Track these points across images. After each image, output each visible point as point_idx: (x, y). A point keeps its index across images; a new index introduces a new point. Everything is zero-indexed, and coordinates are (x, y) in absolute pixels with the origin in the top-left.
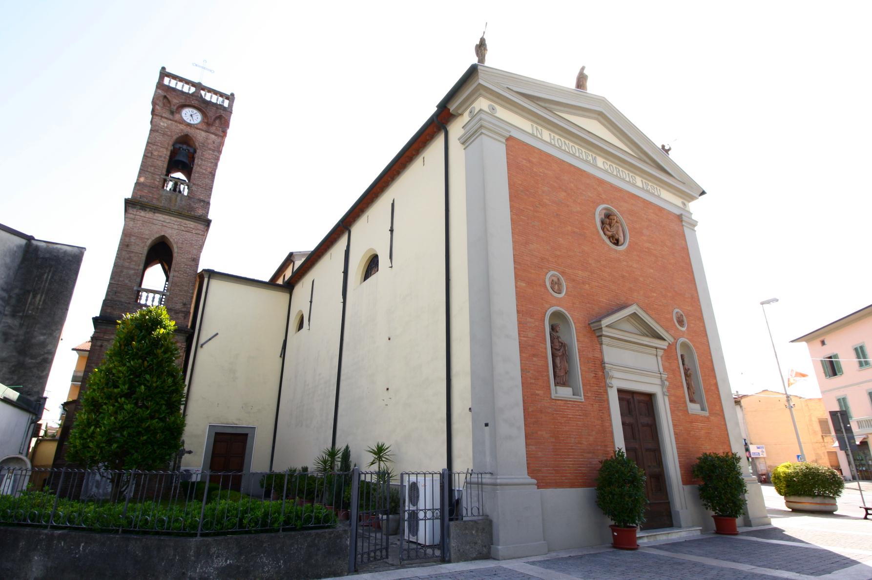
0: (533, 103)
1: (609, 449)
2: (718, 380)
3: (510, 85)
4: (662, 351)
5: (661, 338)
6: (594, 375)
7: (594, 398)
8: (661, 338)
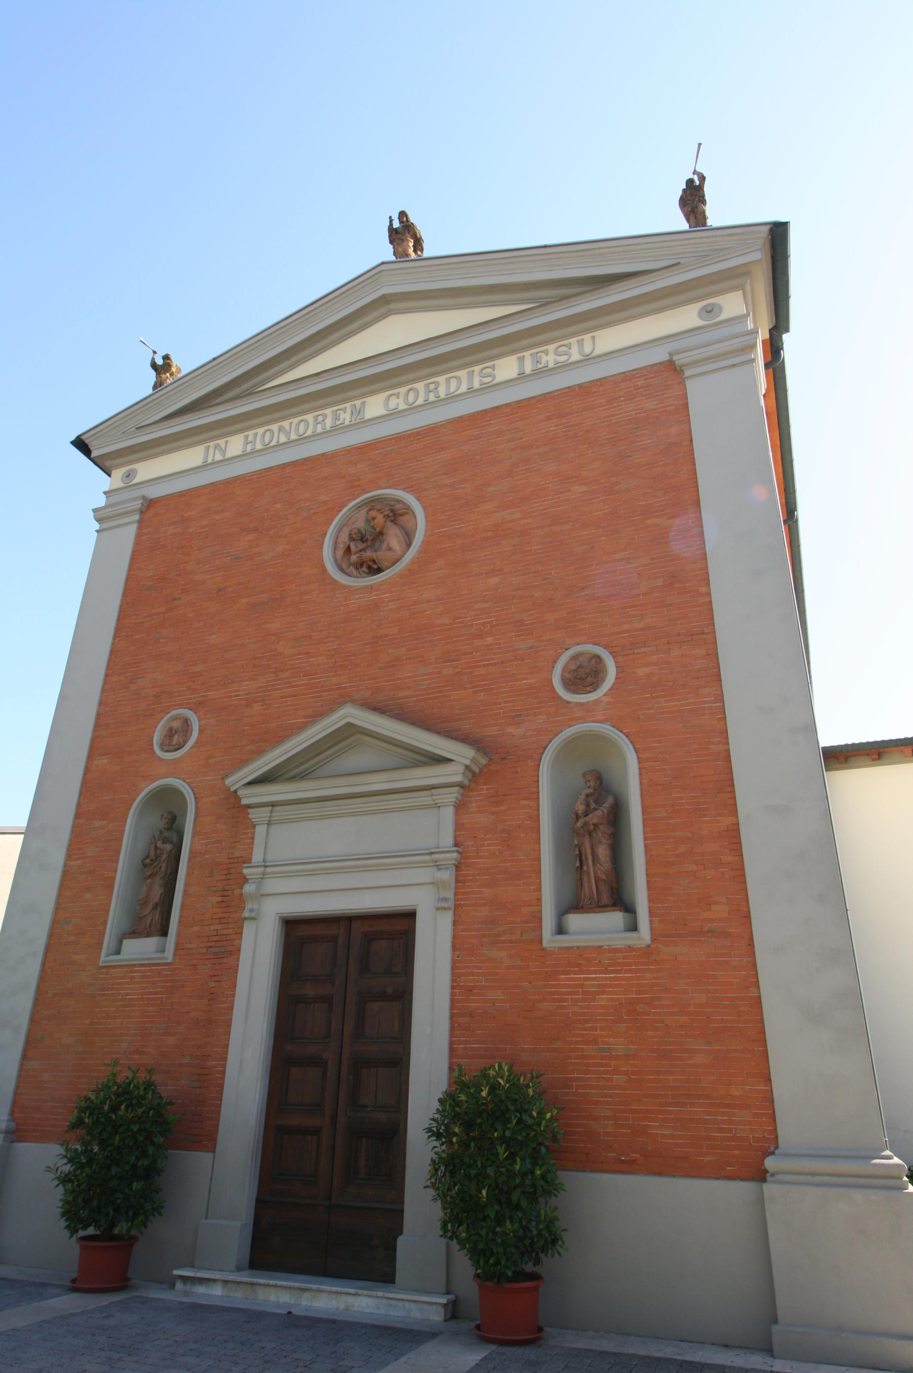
0: (210, 409)
1: (211, 1063)
2: (740, 819)
3: (138, 424)
4: (456, 789)
5: (440, 760)
6: (220, 899)
7: (204, 950)
8: (440, 760)
